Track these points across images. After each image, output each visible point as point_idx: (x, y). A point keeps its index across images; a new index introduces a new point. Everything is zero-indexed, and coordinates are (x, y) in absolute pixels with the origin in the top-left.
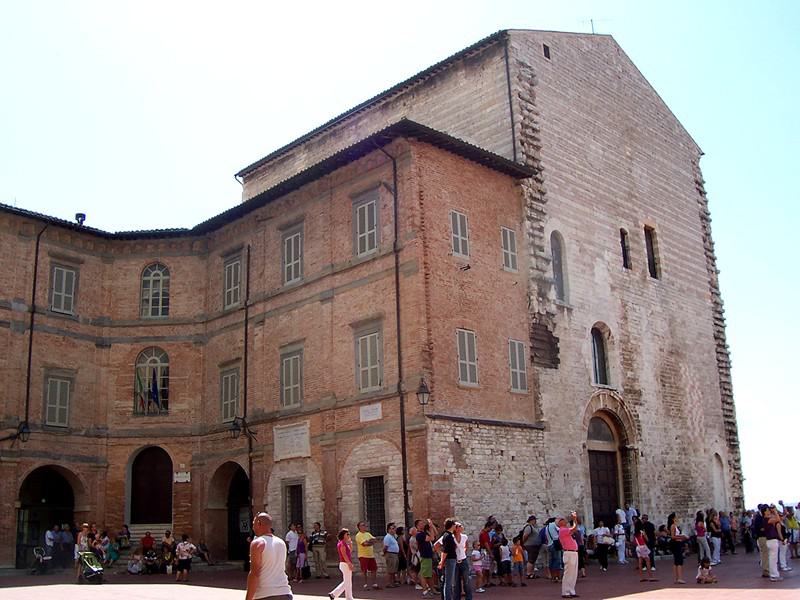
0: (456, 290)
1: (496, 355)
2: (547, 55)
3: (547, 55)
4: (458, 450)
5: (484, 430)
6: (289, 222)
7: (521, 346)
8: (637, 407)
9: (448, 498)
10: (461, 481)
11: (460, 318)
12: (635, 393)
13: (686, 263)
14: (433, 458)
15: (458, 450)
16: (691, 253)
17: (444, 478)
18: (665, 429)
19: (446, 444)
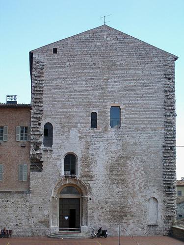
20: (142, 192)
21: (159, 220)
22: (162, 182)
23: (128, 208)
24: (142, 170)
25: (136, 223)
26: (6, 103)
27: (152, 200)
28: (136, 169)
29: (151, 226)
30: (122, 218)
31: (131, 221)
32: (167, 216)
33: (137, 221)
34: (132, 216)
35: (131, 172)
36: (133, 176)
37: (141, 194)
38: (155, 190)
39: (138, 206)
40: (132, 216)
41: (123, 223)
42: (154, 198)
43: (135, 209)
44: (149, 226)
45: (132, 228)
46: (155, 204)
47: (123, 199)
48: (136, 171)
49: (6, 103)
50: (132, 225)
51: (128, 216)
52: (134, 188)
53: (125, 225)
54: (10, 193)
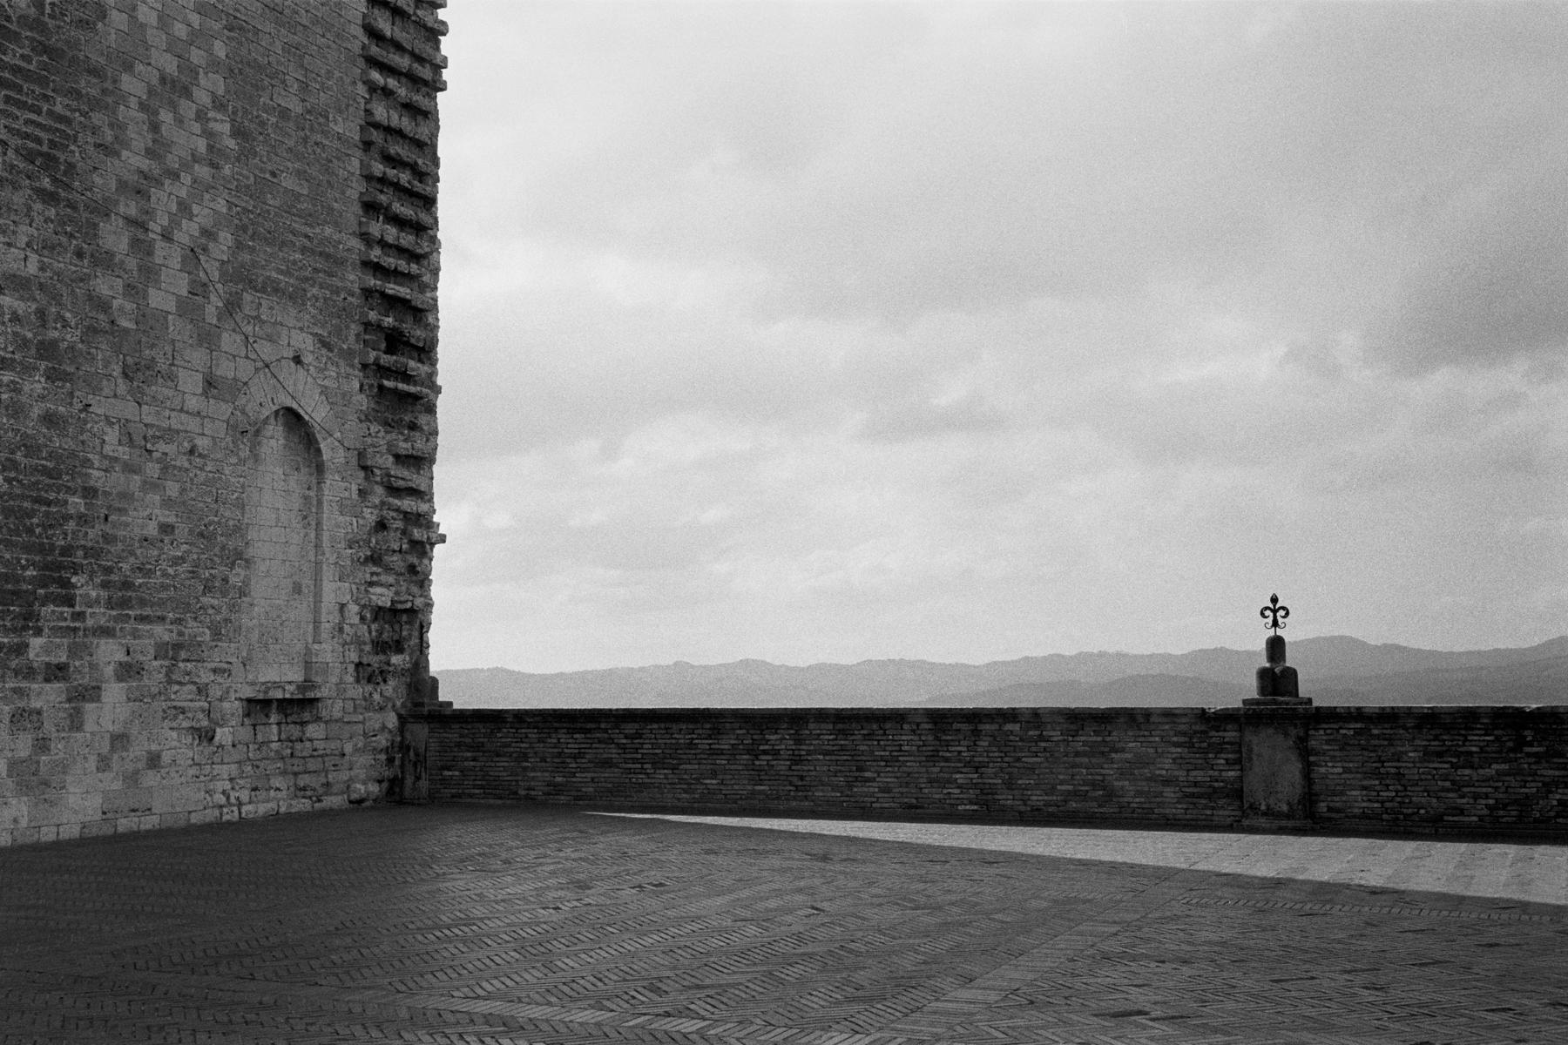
20: (208, 339)
21: (328, 652)
22: (354, 278)
23: (89, 492)
24: (219, 105)
25: (154, 678)
26: (1241, 706)
27: (275, 440)
28: (170, 65)
29: (266, 703)
30: (29, 621)
31: (109, 652)
32: (379, 612)
33: (162, 651)
34: (123, 596)
35: (128, 83)
36: (139, 138)
37: (198, 357)
38: (304, 342)
39: (172, 489)
40: (123, 596)
41: (29, 673)
42: (293, 419)
43: (145, 517)
44: (258, 707)
45: (120, 740)
46: (297, 482)
47: (36, 384)
48: (176, 88)
49: (1241, 706)
50: (114, 692)
51: (85, 587)
52: (150, 273)
53: (47, 697)
54: (1497, 945)
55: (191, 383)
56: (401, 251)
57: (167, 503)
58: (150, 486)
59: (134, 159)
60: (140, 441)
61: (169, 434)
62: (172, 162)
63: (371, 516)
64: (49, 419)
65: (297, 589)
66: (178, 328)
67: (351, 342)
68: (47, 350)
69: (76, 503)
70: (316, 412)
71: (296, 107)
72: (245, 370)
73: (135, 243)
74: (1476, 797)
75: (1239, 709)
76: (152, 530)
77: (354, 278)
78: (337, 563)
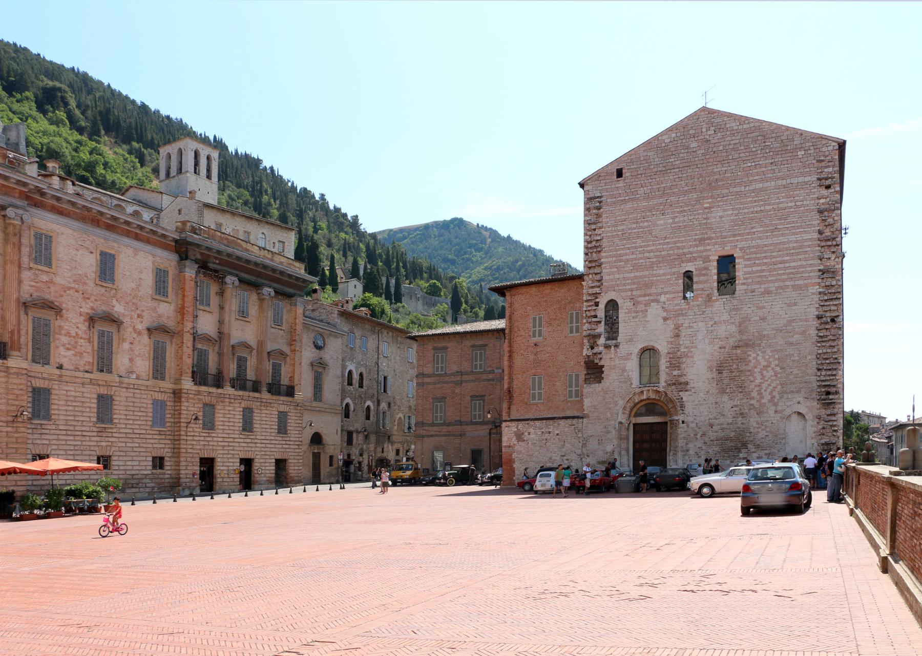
0: (532, 357)
1: (558, 384)
2: (726, 264)
3: (726, 264)
4: (519, 437)
5: (538, 423)
6: (52, 302)
7: (577, 376)
8: (681, 393)
9: (511, 455)
10: (520, 447)
11: (533, 371)
12: (681, 385)
13: (787, 265)
14: (504, 439)
15: (519, 437)
16: (787, 255)
17: (509, 447)
18: (716, 403)
19: (118, 426)
23: (751, 433)
27: (795, 417)
41: (740, 459)
52: (762, 398)
55: (771, 412)
56: (833, 375)
57: (767, 432)
58: (762, 430)
59: (758, 381)
60: (760, 424)
61: (767, 421)
62: (766, 379)
63: (820, 427)
64: (742, 424)
65: (801, 442)
66: (768, 405)
67: (815, 396)
68: (742, 414)
69: (748, 434)
70: (803, 410)
71: (777, 362)
72: (784, 407)
73: (758, 394)
74: (627, 260)
75: (151, 110)
76: (764, 436)
77: (815, 384)
78: (644, 479)
